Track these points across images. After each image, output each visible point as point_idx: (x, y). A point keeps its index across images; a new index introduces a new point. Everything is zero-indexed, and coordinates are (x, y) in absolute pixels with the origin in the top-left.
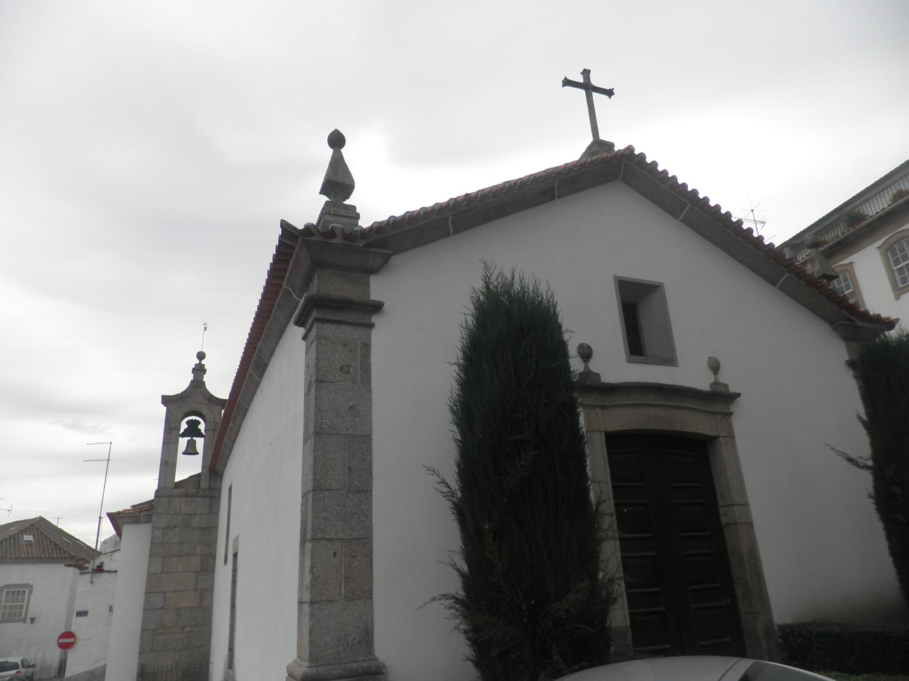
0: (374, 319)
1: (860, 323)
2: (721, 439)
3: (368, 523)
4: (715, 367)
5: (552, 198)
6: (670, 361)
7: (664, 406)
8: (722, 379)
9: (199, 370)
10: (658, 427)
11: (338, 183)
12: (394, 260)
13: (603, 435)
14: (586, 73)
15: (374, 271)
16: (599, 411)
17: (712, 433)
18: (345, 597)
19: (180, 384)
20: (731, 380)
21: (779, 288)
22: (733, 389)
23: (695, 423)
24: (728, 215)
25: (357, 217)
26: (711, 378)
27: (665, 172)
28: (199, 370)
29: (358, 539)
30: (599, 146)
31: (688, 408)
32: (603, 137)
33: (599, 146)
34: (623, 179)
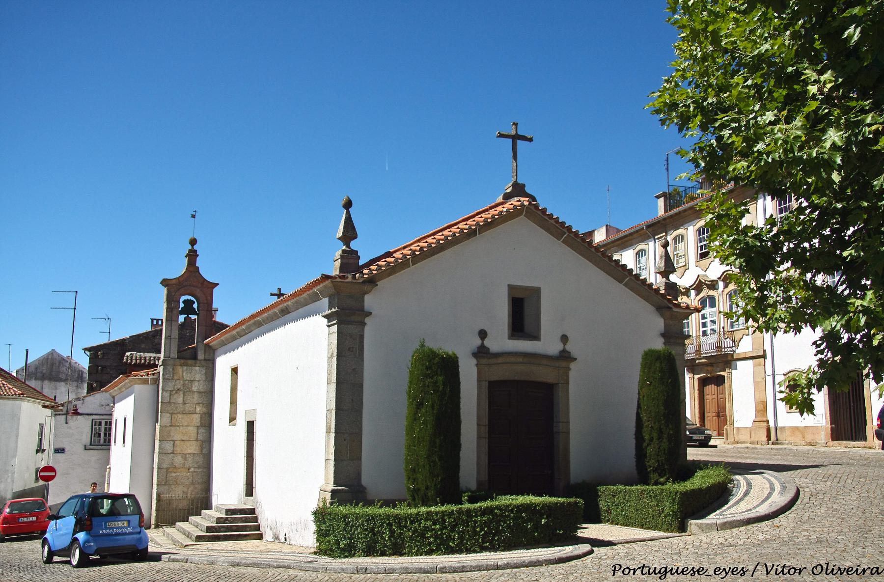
0: (367, 320)
4: (564, 339)
6: (536, 337)
9: (192, 256)
14: (280, 289)
19: (178, 269)
23: (545, 374)
25: (359, 258)
28: (192, 256)
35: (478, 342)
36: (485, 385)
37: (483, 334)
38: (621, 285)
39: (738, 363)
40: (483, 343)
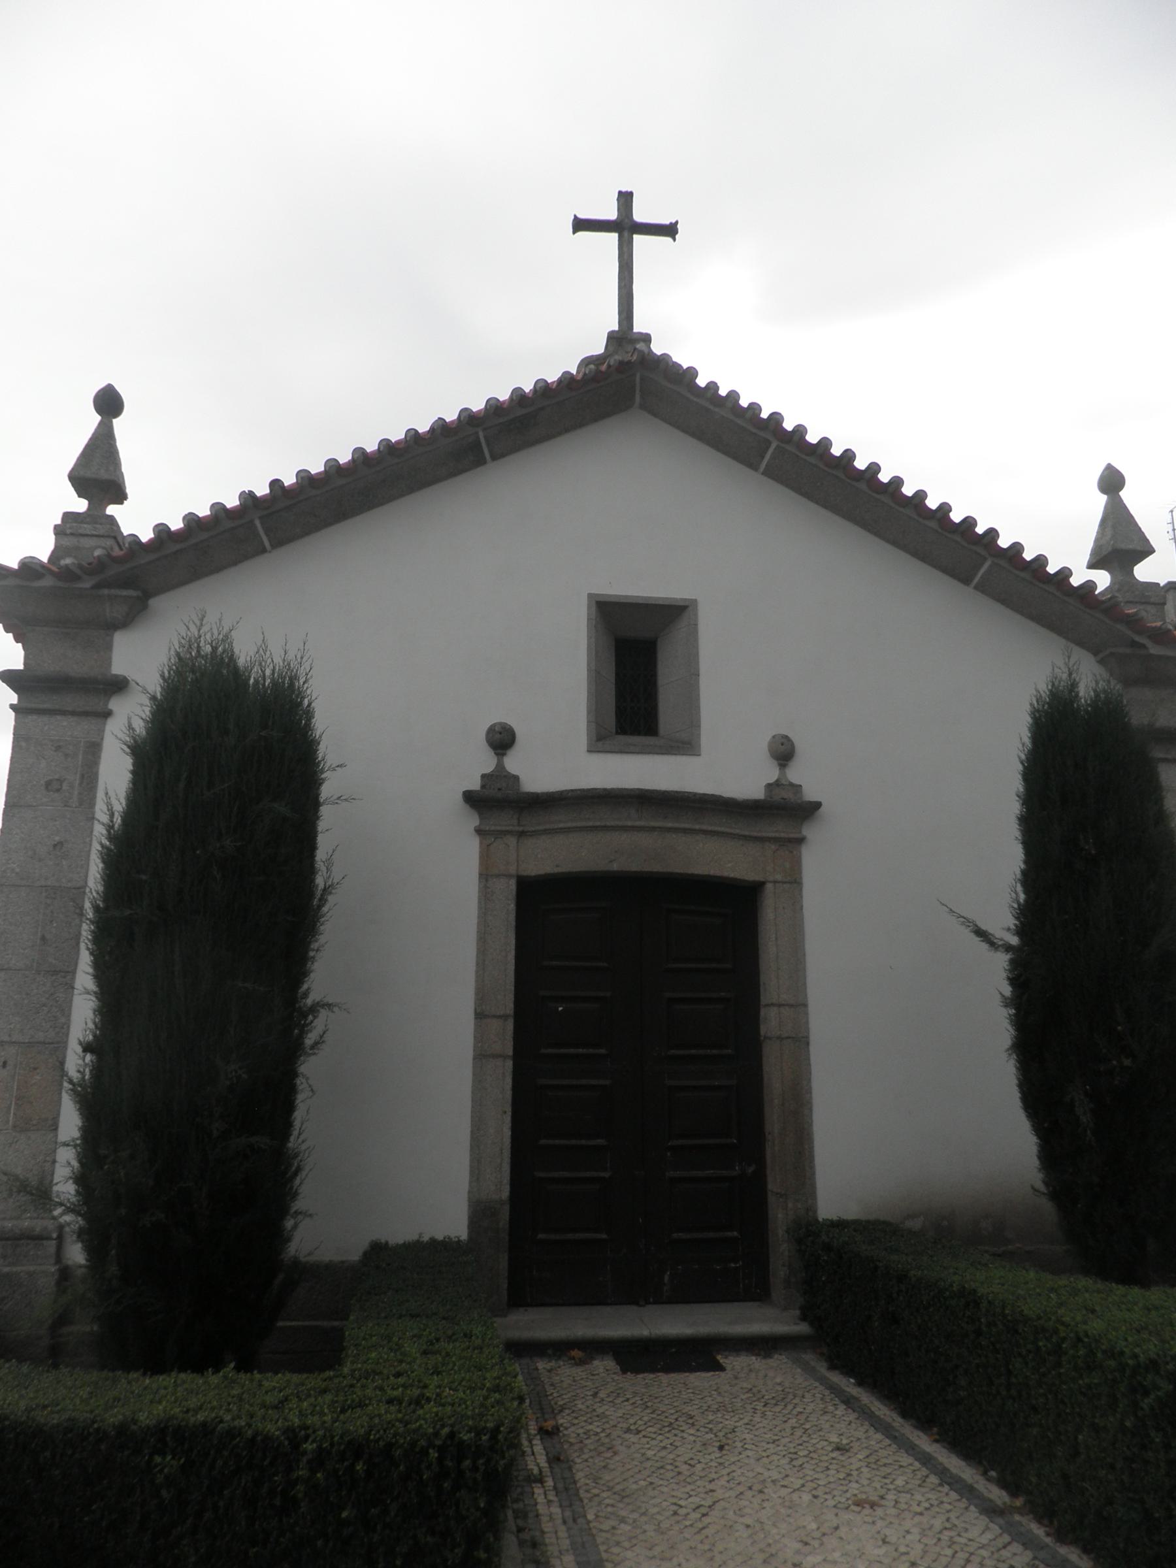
0: (114, 704)
1: (1154, 650)
2: (769, 886)
3: (63, 1020)
4: (783, 752)
5: (480, 462)
7: (653, 829)
8: (795, 774)
10: (634, 866)
11: (98, 475)
12: (153, 602)
13: (513, 884)
14: (625, 199)
15: (125, 623)
16: (512, 841)
17: (751, 876)
18: (14, 1127)
20: (808, 778)
21: (976, 588)
22: (811, 794)
24: (218, 508)
26: (771, 773)
27: (713, 386)
29: (44, 1043)
30: (626, 340)
31: (705, 832)
32: (638, 327)
33: (626, 340)
34: (643, 407)
35: (486, 762)
36: (507, 890)
37: (502, 740)
38: (969, 590)
39: (637, 328)
40: (500, 766)
